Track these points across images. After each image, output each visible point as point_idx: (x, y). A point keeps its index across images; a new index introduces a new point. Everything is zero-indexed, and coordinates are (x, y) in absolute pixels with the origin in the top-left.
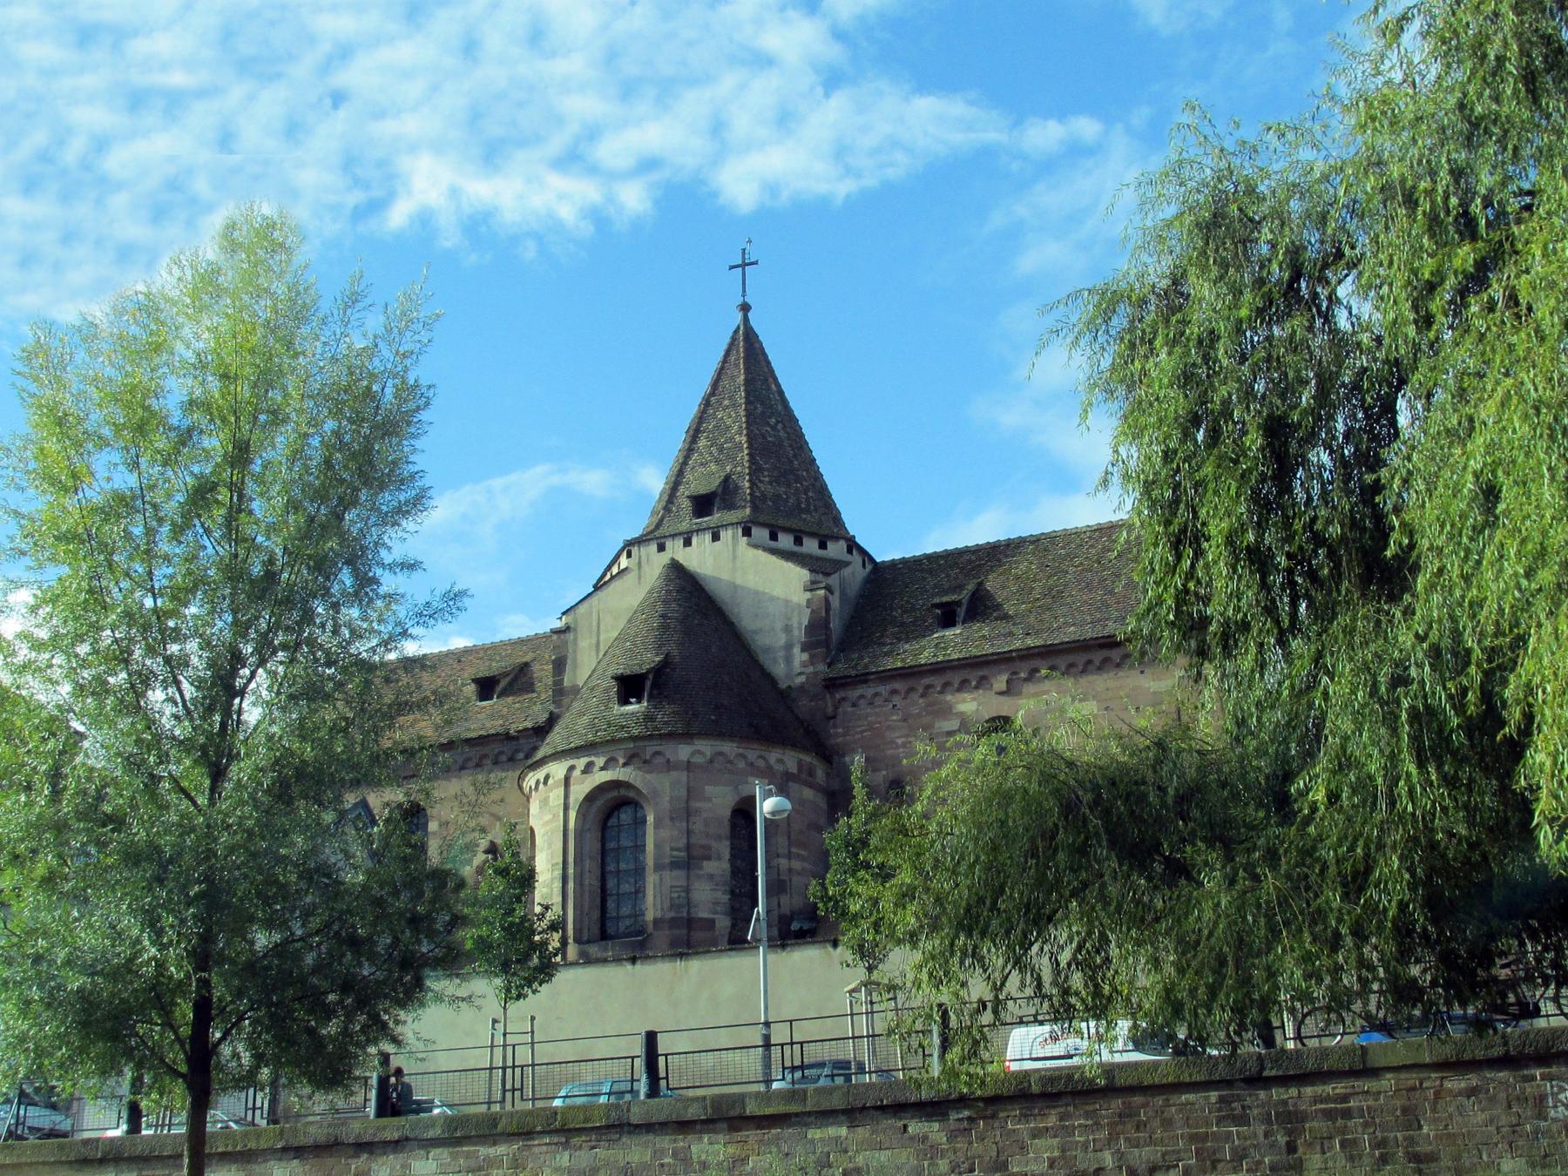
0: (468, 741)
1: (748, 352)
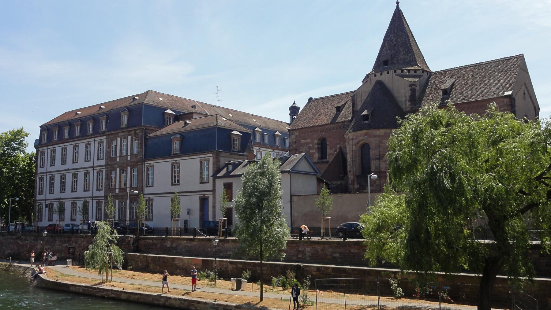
1: (398, 22)
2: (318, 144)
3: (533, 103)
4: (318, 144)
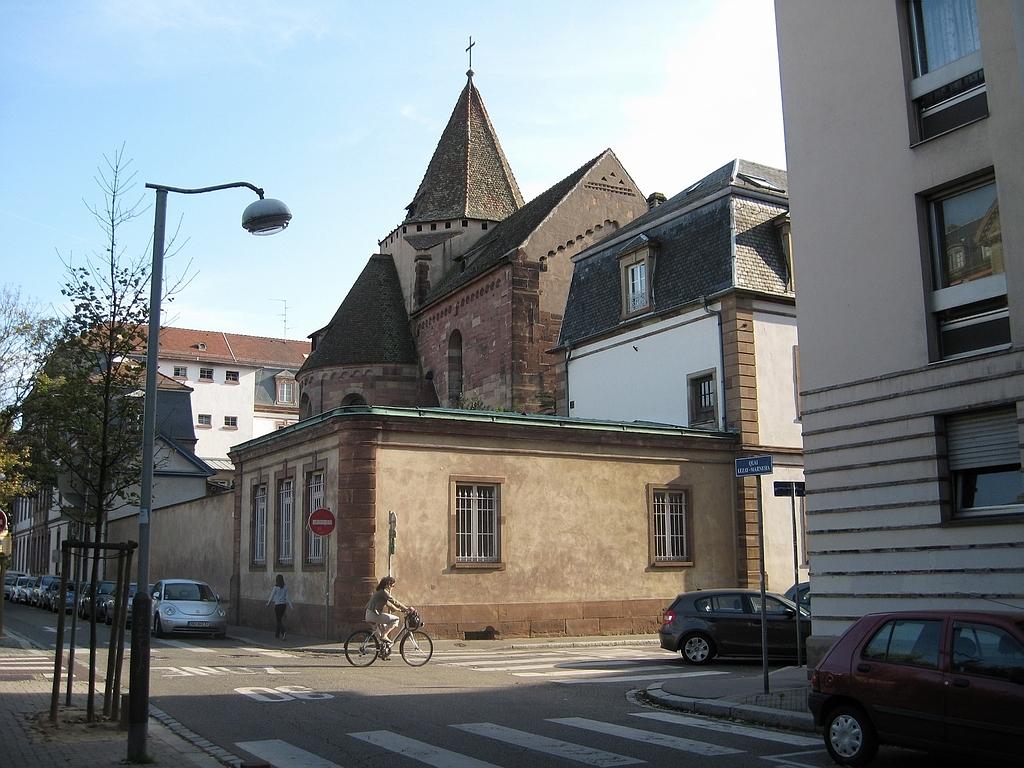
1: (469, 102)
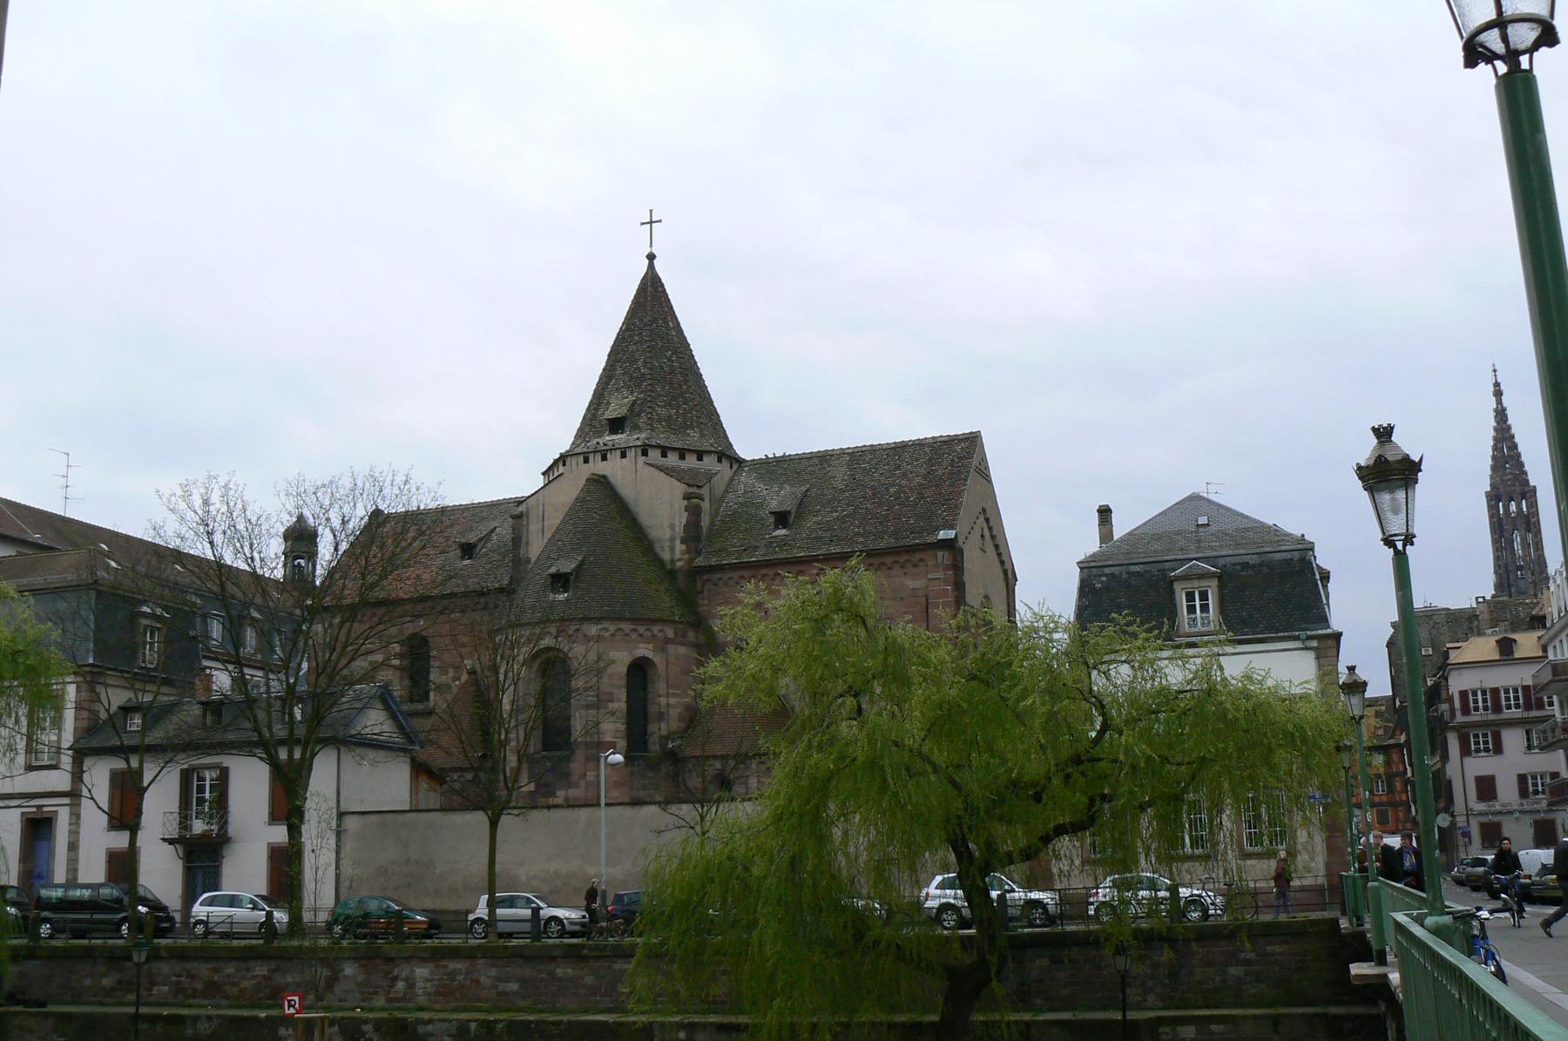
0: (465, 595)
1: (651, 306)
2: (400, 656)
3: (1002, 563)
4: (400, 656)
